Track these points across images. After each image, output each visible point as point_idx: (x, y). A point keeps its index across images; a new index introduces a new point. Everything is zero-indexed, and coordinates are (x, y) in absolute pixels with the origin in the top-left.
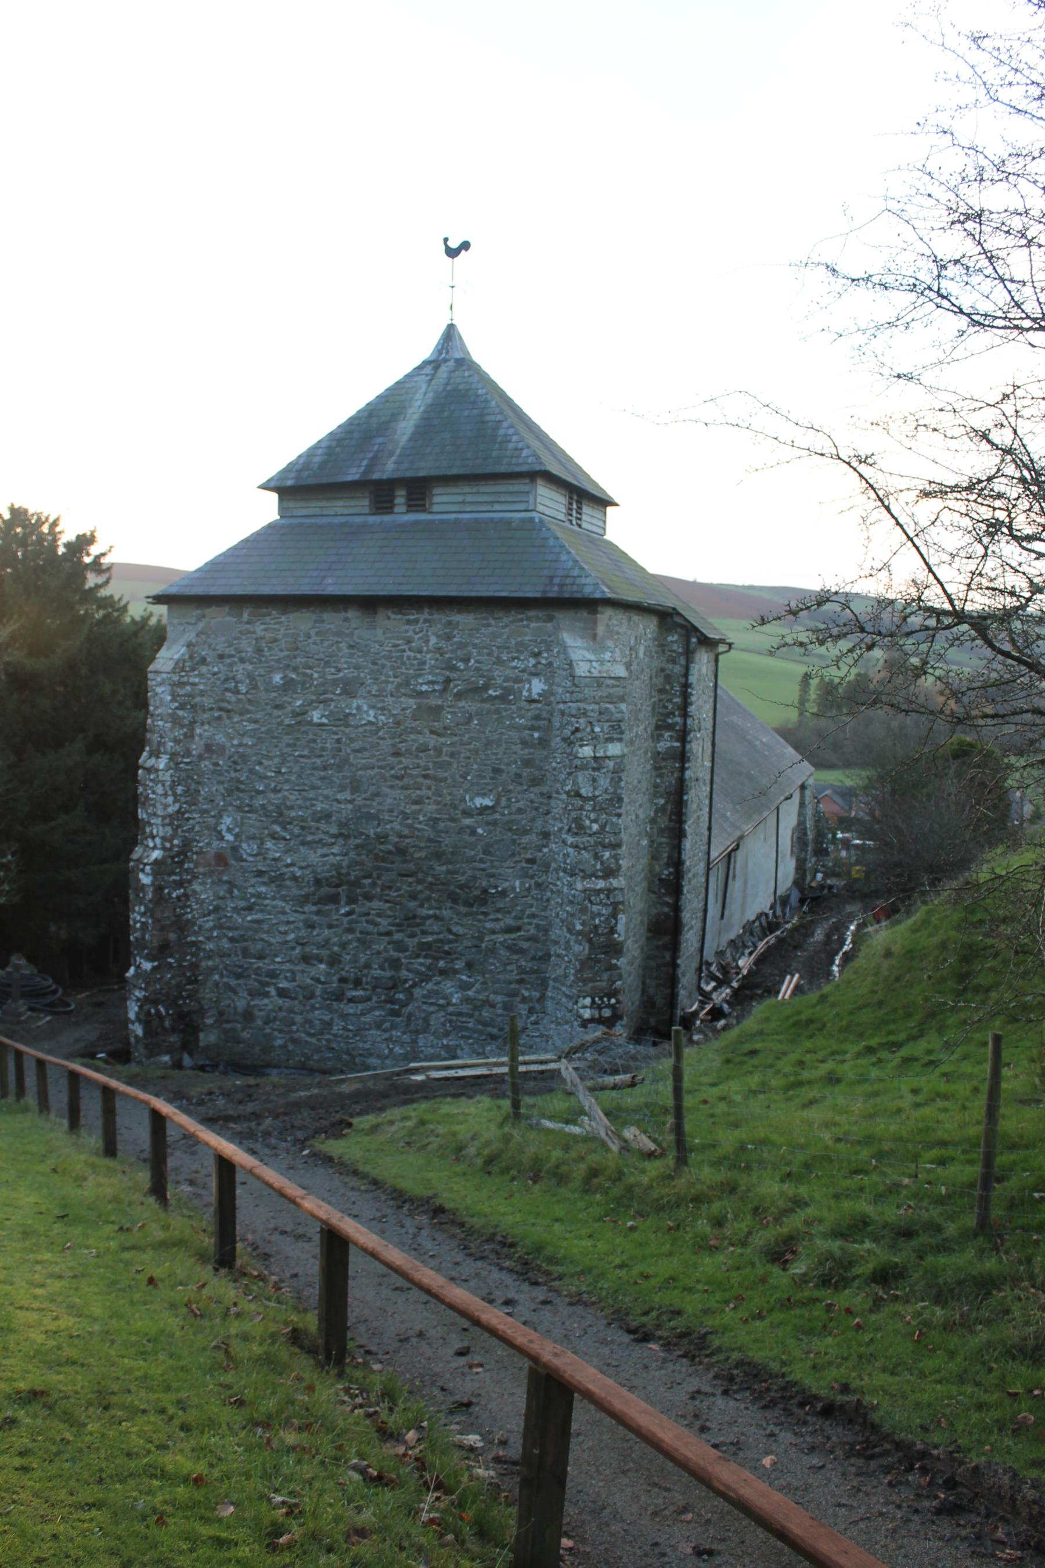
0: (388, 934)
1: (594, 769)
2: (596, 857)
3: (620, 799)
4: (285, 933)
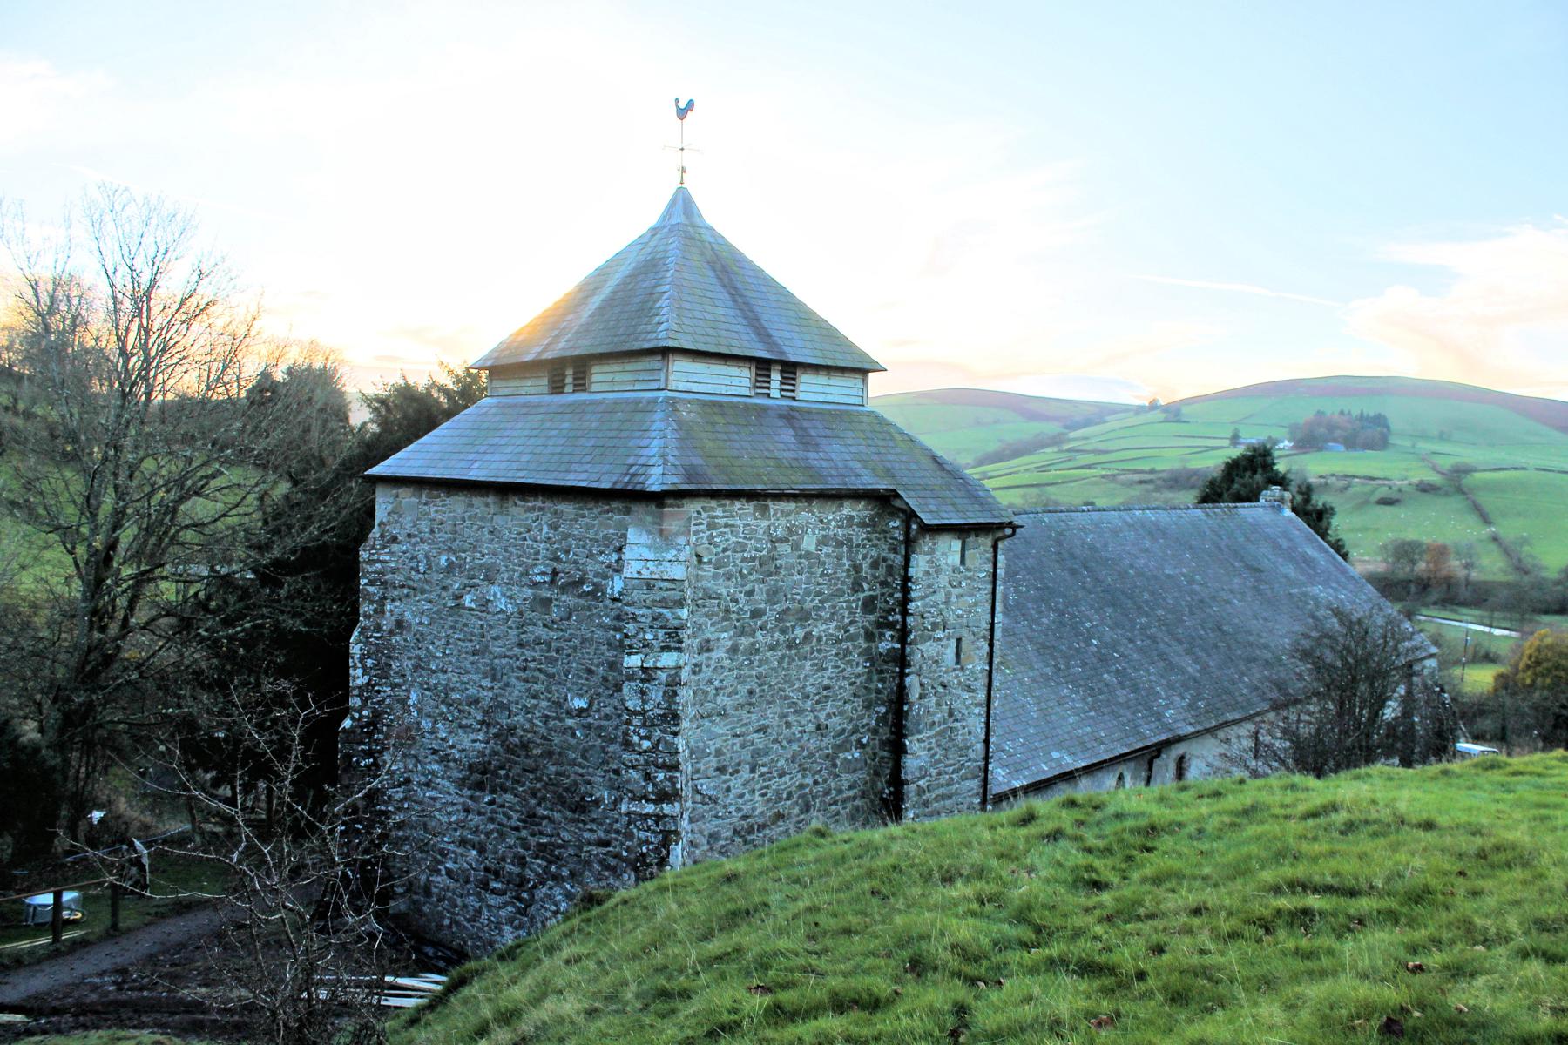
0: (517, 829)
1: (642, 681)
2: (648, 777)
3: (676, 717)
4: (449, 814)
